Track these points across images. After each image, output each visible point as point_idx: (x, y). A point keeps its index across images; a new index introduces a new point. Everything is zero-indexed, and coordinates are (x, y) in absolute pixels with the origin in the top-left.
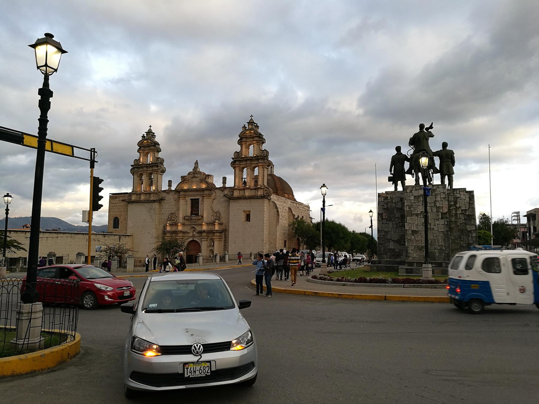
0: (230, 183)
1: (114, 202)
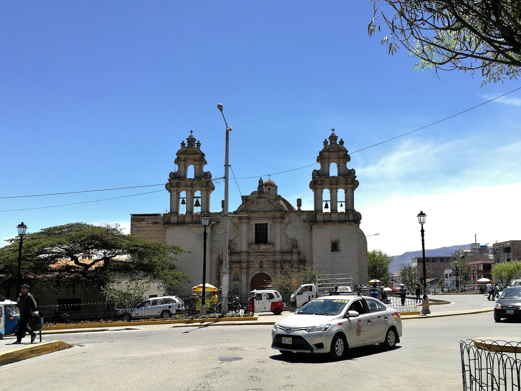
0: (308, 206)
1: (139, 225)
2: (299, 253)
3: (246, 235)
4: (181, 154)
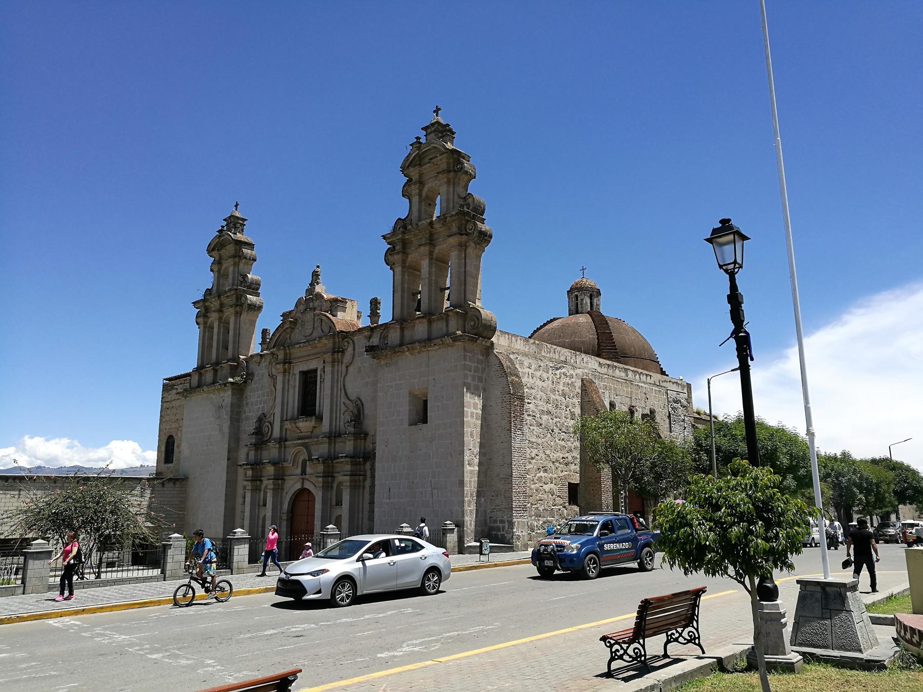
4: (213, 250)
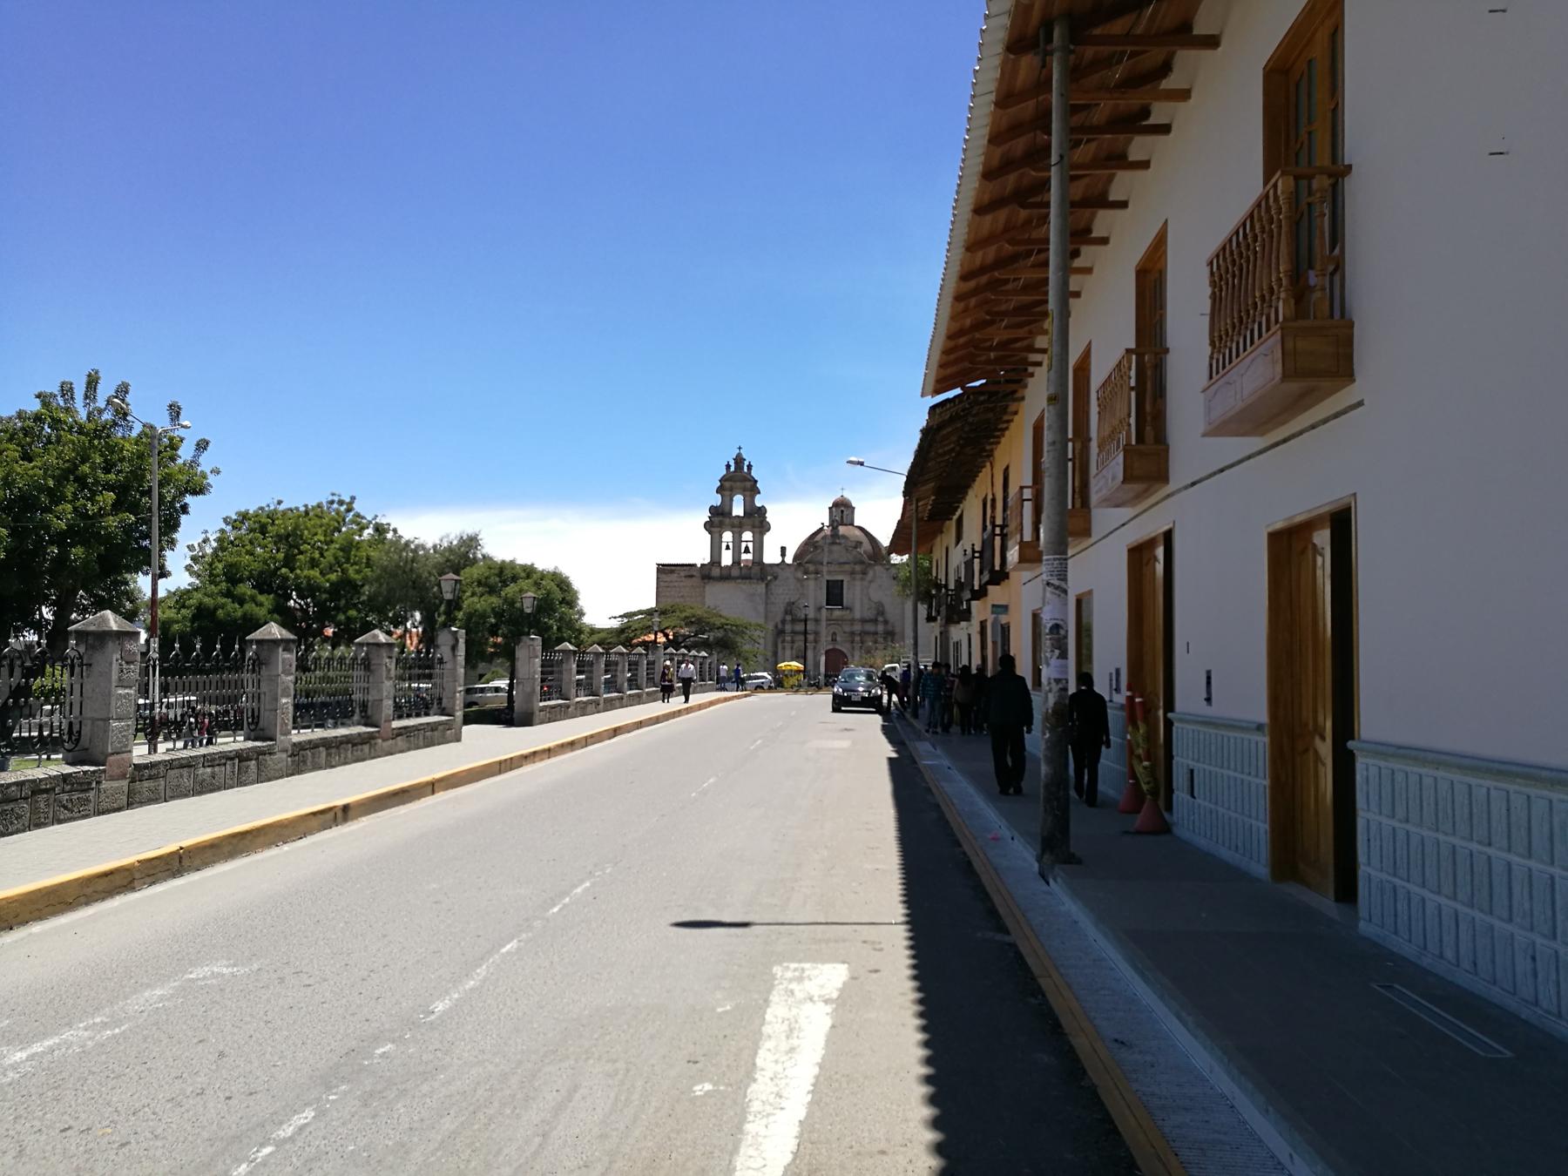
2: (886, 622)
3: (815, 594)
